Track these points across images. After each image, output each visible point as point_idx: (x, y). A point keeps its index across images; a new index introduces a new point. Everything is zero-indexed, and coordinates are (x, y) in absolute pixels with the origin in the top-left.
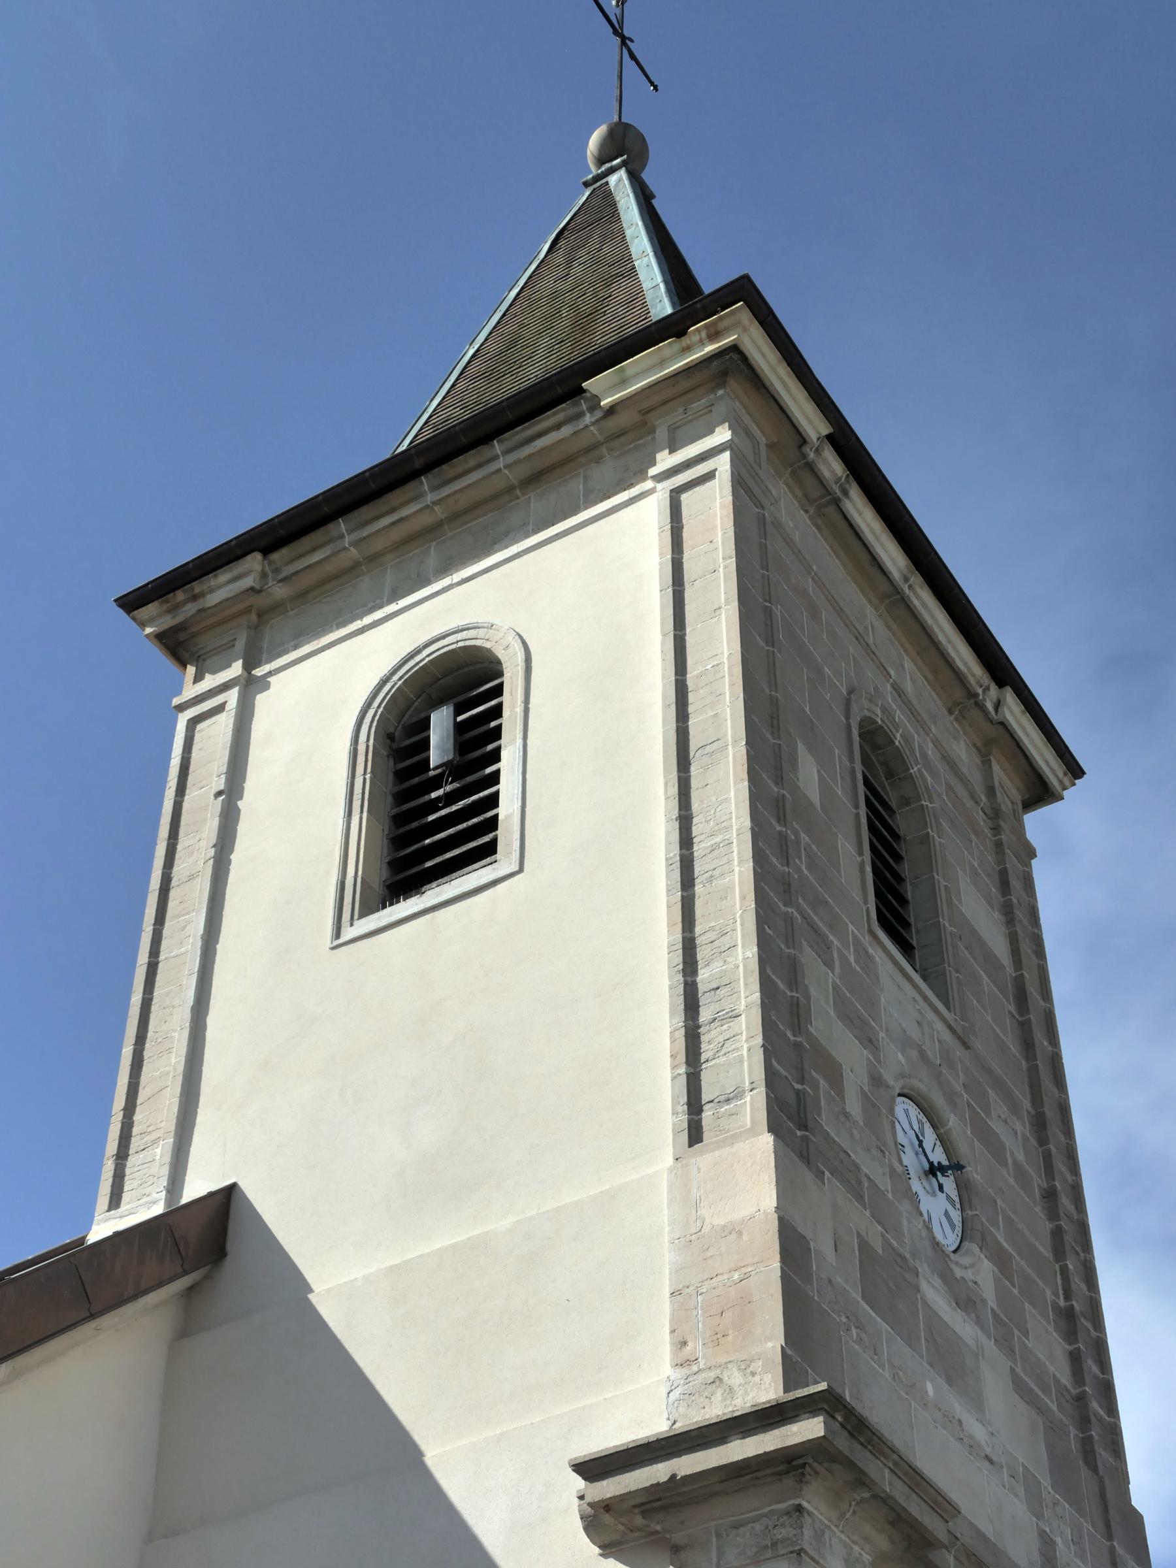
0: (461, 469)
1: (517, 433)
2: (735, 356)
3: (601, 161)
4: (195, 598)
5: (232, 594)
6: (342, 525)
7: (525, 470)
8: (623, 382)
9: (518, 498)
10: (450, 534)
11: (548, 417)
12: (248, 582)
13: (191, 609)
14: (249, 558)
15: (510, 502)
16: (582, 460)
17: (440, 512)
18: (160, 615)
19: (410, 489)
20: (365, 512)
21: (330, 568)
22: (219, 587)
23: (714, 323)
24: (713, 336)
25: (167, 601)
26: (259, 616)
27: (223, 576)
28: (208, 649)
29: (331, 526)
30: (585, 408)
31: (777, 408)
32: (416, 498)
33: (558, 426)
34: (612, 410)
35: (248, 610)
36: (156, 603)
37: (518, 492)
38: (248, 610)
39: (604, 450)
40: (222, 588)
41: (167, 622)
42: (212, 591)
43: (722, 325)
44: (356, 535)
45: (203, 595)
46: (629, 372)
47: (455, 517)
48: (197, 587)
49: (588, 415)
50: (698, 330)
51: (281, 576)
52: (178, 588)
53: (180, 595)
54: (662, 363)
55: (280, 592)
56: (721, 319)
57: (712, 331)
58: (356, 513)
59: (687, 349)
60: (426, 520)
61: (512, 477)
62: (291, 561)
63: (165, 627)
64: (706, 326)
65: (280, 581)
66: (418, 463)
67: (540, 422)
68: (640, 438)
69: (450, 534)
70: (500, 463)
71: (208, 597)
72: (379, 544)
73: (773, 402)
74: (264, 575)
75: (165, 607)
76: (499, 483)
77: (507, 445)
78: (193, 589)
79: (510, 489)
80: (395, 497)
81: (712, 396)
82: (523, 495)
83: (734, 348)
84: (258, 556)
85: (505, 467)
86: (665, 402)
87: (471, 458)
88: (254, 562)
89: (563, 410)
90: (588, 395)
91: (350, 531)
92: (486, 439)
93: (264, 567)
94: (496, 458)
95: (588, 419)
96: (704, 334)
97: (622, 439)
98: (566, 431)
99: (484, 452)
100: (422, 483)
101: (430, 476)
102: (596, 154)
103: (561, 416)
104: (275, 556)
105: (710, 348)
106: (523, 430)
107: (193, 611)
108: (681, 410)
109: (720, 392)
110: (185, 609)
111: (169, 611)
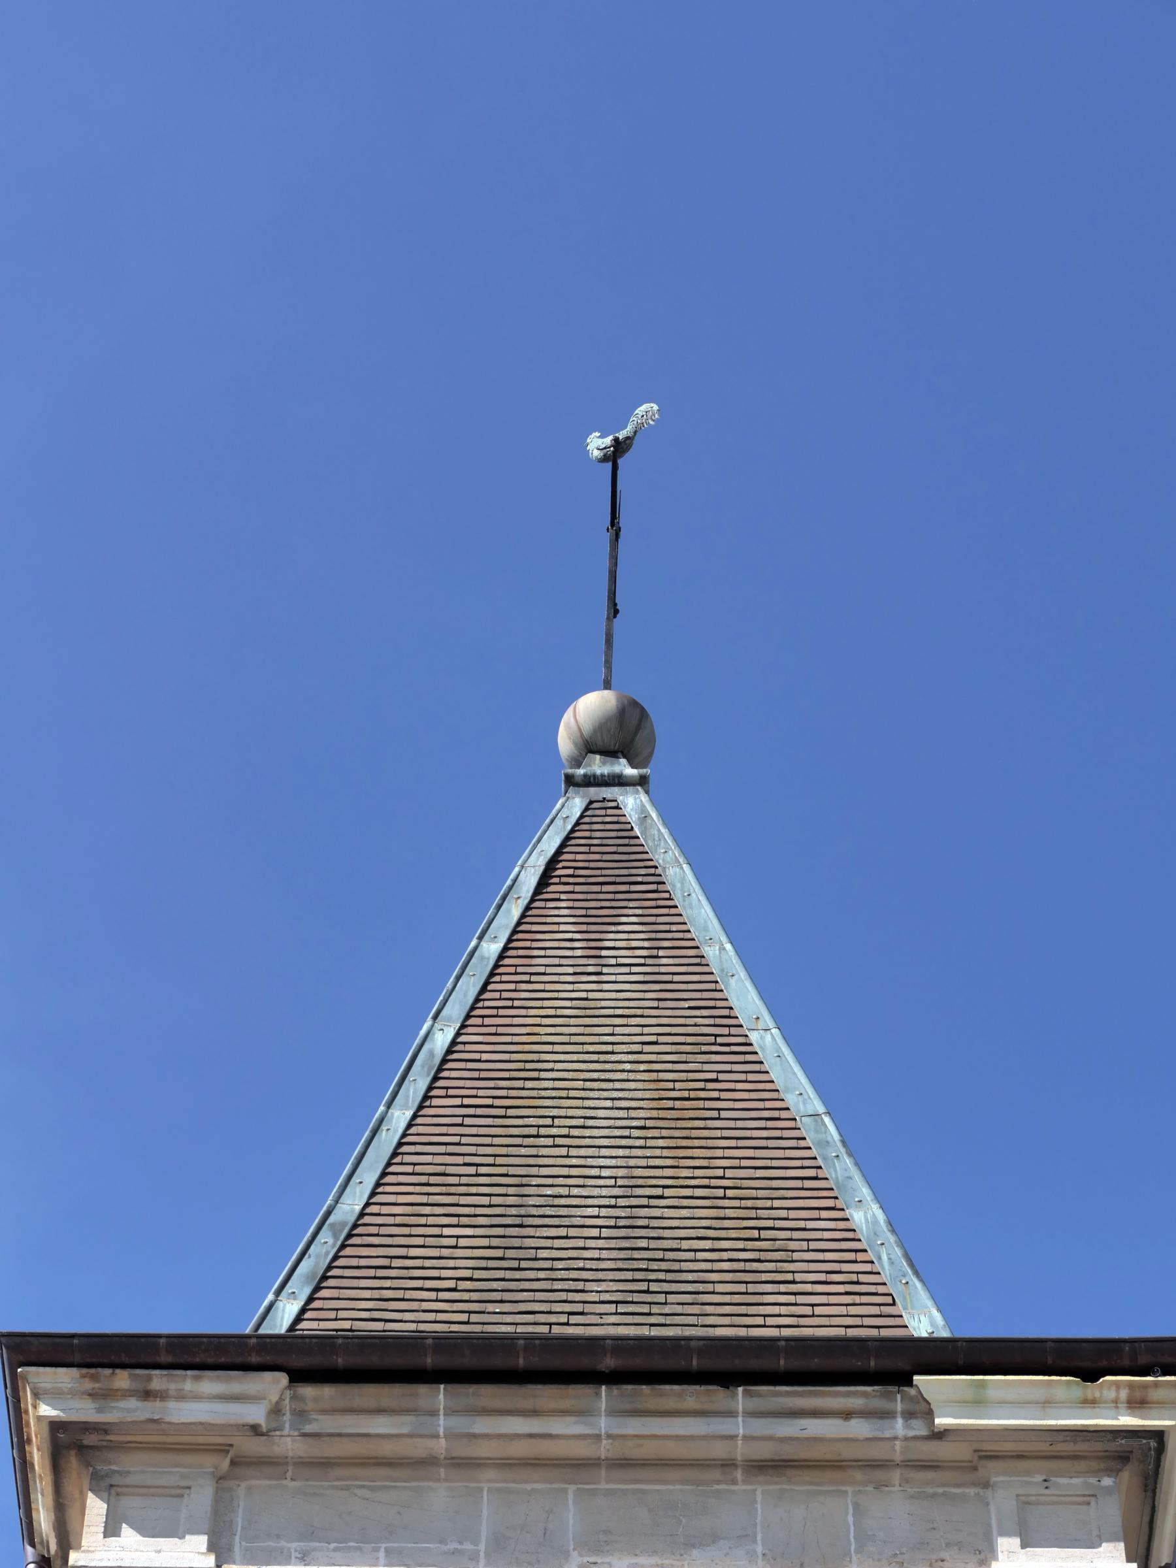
0: (671, 1403)
1: (780, 1394)
2: (1153, 1444)
3: (589, 746)
4: (147, 1395)
5: (220, 1420)
6: (441, 1396)
7: (765, 1451)
8: (978, 1404)
9: (734, 1482)
10: (603, 1486)
11: (836, 1394)
12: (256, 1414)
13: (130, 1410)
14: (268, 1375)
15: (718, 1482)
16: (858, 1475)
17: (604, 1449)
18: (73, 1393)
19: (576, 1395)
20: (487, 1394)
21: (388, 1449)
22: (197, 1397)
23: (1145, 1386)
24: (1137, 1403)
25: (94, 1378)
26: (233, 1463)
27: (211, 1384)
28: (129, 1480)
29: (423, 1389)
30: (899, 1409)
31: (1146, 1519)
32: (580, 1413)
33: (847, 1415)
34: (940, 1435)
35: (223, 1449)
36: (74, 1372)
37: (739, 1474)
38: (223, 1449)
39: (896, 1476)
40: (203, 1403)
41: (84, 1411)
42: (181, 1397)
43: (1155, 1395)
44: (460, 1423)
45: (162, 1396)
46: (992, 1394)
47: (622, 1464)
48: (158, 1380)
49: (900, 1421)
50: (1118, 1385)
51: (308, 1428)
52: (123, 1366)
53: (122, 1379)
54: (1046, 1405)
55: (288, 1444)
56: (1156, 1385)
57: (1138, 1395)
58: (472, 1389)
59: (1090, 1403)
60: (582, 1450)
61: (741, 1451)
62: (333, 1411)
63: (74, 1417)
64: (1130, 1385)
65: (304, 1435)
66: (609, 1363)
67: (822, 1394)
68: (957, 1486)
69: (603, 1486)
70: (739, 1426)
71: (171, 1404)
72: (483, 1450)
73: (1148, 1510)
74: (276, 1411)
75: (88, 1385)
76: (719, 1450)
77: (756, 1404)
78: (149, 1379)
79: (728, 1465)
80: (546, 1395)
81: (1093, 1480)
82: (744, 1482)
83: (1159, 1435)
84: (283, 1379)
85: (745, 1437)
86: (1020, 1457)
87: (691, 1396)
88: (274, 1384)
89: (865, 1395)
90: (912, 1392)
91: (450, 1412)
92: (727, 1379)
93: (281, 1399)
94: (731, 1414)
95: (899, 1427)
96: (1124, 1394)
97: (930, 1475)
98: (859, 1428)
99: (716, 1396)
100: (598, 1395)
101: (616, 1390)
102: (587, 728)
103: (856, 1403)
104: (308, 1391)
105: (1127, 1420)
106: (788, 1394)
107: (141, 1416)
108: (1039, 1478)
109: (1107, 1481)
110: (122, 1404)
111: (92, 1395)
